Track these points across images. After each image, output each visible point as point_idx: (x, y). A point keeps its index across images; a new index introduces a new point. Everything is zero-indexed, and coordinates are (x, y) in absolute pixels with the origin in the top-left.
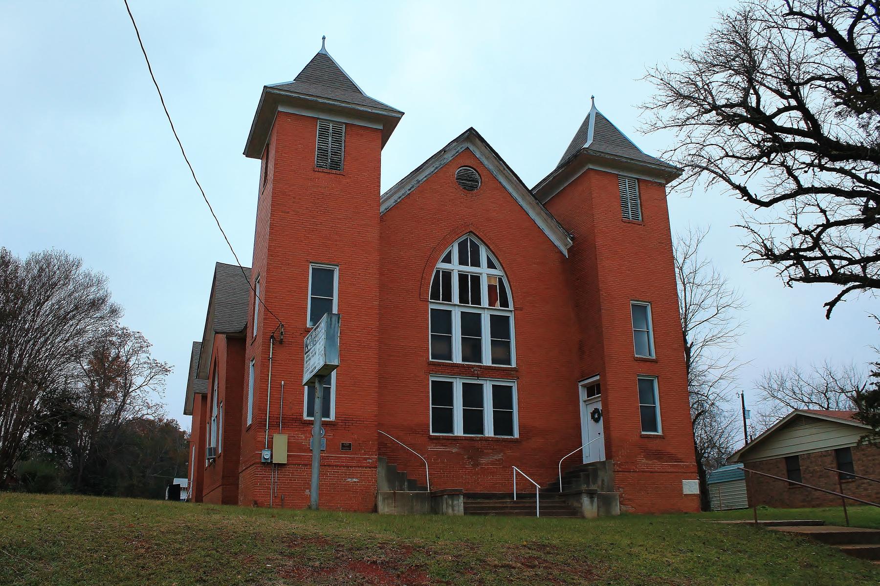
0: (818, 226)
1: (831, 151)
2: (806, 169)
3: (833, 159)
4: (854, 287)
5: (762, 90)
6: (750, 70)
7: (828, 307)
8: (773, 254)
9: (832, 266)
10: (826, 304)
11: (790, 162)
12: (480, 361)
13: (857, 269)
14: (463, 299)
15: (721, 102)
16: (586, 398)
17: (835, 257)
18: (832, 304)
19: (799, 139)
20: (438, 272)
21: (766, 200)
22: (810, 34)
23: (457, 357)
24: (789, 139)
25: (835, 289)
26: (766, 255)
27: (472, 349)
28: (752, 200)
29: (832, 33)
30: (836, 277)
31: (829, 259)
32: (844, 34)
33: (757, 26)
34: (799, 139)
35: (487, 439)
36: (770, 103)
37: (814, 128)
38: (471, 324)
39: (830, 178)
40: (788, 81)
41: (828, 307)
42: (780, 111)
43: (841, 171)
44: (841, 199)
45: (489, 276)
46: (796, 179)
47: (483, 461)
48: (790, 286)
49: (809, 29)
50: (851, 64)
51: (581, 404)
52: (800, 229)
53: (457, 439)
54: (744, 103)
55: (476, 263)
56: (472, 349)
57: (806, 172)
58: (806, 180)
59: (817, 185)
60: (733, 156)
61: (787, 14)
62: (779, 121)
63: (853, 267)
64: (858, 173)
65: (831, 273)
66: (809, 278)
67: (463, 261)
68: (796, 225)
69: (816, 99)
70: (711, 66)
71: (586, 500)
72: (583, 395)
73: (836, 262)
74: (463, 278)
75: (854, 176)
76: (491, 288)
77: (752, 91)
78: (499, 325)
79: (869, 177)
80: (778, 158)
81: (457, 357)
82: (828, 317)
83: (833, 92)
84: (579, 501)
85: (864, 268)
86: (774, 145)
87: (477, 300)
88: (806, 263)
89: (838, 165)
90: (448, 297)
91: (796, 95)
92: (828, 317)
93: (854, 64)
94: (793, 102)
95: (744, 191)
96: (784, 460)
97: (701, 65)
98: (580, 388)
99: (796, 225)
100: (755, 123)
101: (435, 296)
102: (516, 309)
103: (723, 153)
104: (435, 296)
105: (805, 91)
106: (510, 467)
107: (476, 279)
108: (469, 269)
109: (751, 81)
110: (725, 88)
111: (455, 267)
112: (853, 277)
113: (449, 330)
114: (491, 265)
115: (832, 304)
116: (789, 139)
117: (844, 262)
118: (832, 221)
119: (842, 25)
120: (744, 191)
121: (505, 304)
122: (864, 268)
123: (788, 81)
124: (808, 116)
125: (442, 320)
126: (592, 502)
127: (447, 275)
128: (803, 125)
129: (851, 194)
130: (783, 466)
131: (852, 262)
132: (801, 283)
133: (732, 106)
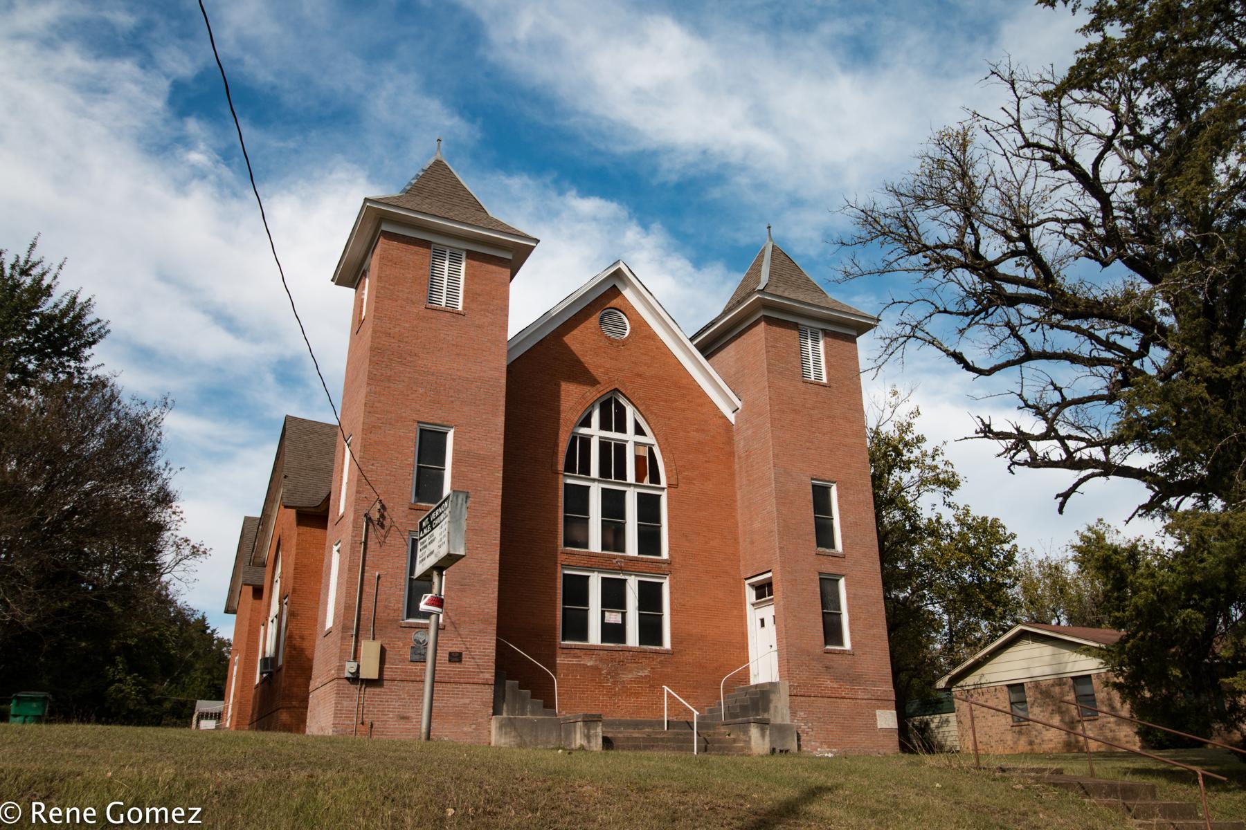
0: (1052, 406)
1: (1065, 307)
2: (1033, 326)
3: (1067, 316)
4: (1093, 475)
5: (982, 231)
6: (967, 206)
7: (1060, 499)
8: (991, 431)
9: (1066, 449)
10: (1058, 496)
11: (1015, 321)
12: (623, 550)
13: (1097, 453)
14: (605, 472)
15: (930, 242)
16: (753, 599)
17: (1070, 437)
18: (1066, 496)
19: (1023, 290)
20: (574, 439)
21: (986, 367)
22: (1047, 165)
23: (595, 544)
24: (1010, 289)
25: (1068, 477)
26: (984, 432)
27: (613, 535)
28: (968, 367)
29: (1072, 165)
30: (1070, 462)
31: (1062, 440)
32: (1087, 167)
33: (1131, 343)
34: (1023, 290)
35: (630, 650)
36: (992, 247)
37: (1046, 274)
38: (614, 504)
39: (1065, 340)
40: (1018, 223)
41: (1060, 499)
42: (1005, 257)
43: (1078, 330)
44: (1078, 367)
45: (637, 444)
46: (1023, 342)
47: (627, 677)
48: (1011, 472)
49: (1044, 159)
50: (1094, 202)
51: (749, 608)
52: (1025, 401)
53: (593, 649)
54: (959, 245)
55: (621, 428)
56: (613, 535)
57: (1033, 331)
58: (1035, 340)
59: (1048, 350)
60: (945, 311)
61: (1022, 147)
62: (1002, 269)
63: (1092, 449)
64: (1097, 333)
65: (1064, 456)
66: (1036, 462)
67: (605, 425)
68: (1020, 396)
69: (1048, 242)
70: (920, 200)
71: (754, 732)
72: (750, 595)
73: (1072, 444)
74: (604, 445)
75: (1092, 337)
76: (639, 460)
77: (969, 230)
78: (649, 507)
79: (1112, 339)
80: (1001, 314)
81: (595, 544)
82: (1061, 511)
83: (1072, 239)
84: (746, 732)
85: (1107, 452)
86: (992, 297)
87: (621, 474)
88: (1032, 443)
89: (1072, 323)
90: (586, 469)
91: (1025, 238)
92: (1061, 511)
93: (1099, 205)
94: (1021, 246)
95: (959, 358)
96: (1006, 689)
97: (903, 199)
98: (747, 587)
99: (1020, 396)
100: (973, 269)
101: (570, 467)
102: (670, 486)
103: (931, 309)
104: (570, 467)
105: (1035, 234)
106: (660, 686)
107: (621, 449)
108: (612, 435)
109: (968, 217)
110: (938, 226)
111: (595, 431)
112: (1092, 463)
113: (586, 510)
114: (639, 431)
115: (1066, 496)
116: (1010, 289)
117: (1083, 444)
118: (1069, 398)
119: (1085, 156)
120: (959, 358)
121: (655, 478)
122: (1107, 452)
123: (1018, 223)
124: (1038, 262)
125: (578, 498)
126: (763, 736)
127: (586, 441)
128: (1031, 274)
129: (1092, 362)
130: (1003, 701)
131: (1091, 444)
132: (1026, 467)
133: (945, 247)
